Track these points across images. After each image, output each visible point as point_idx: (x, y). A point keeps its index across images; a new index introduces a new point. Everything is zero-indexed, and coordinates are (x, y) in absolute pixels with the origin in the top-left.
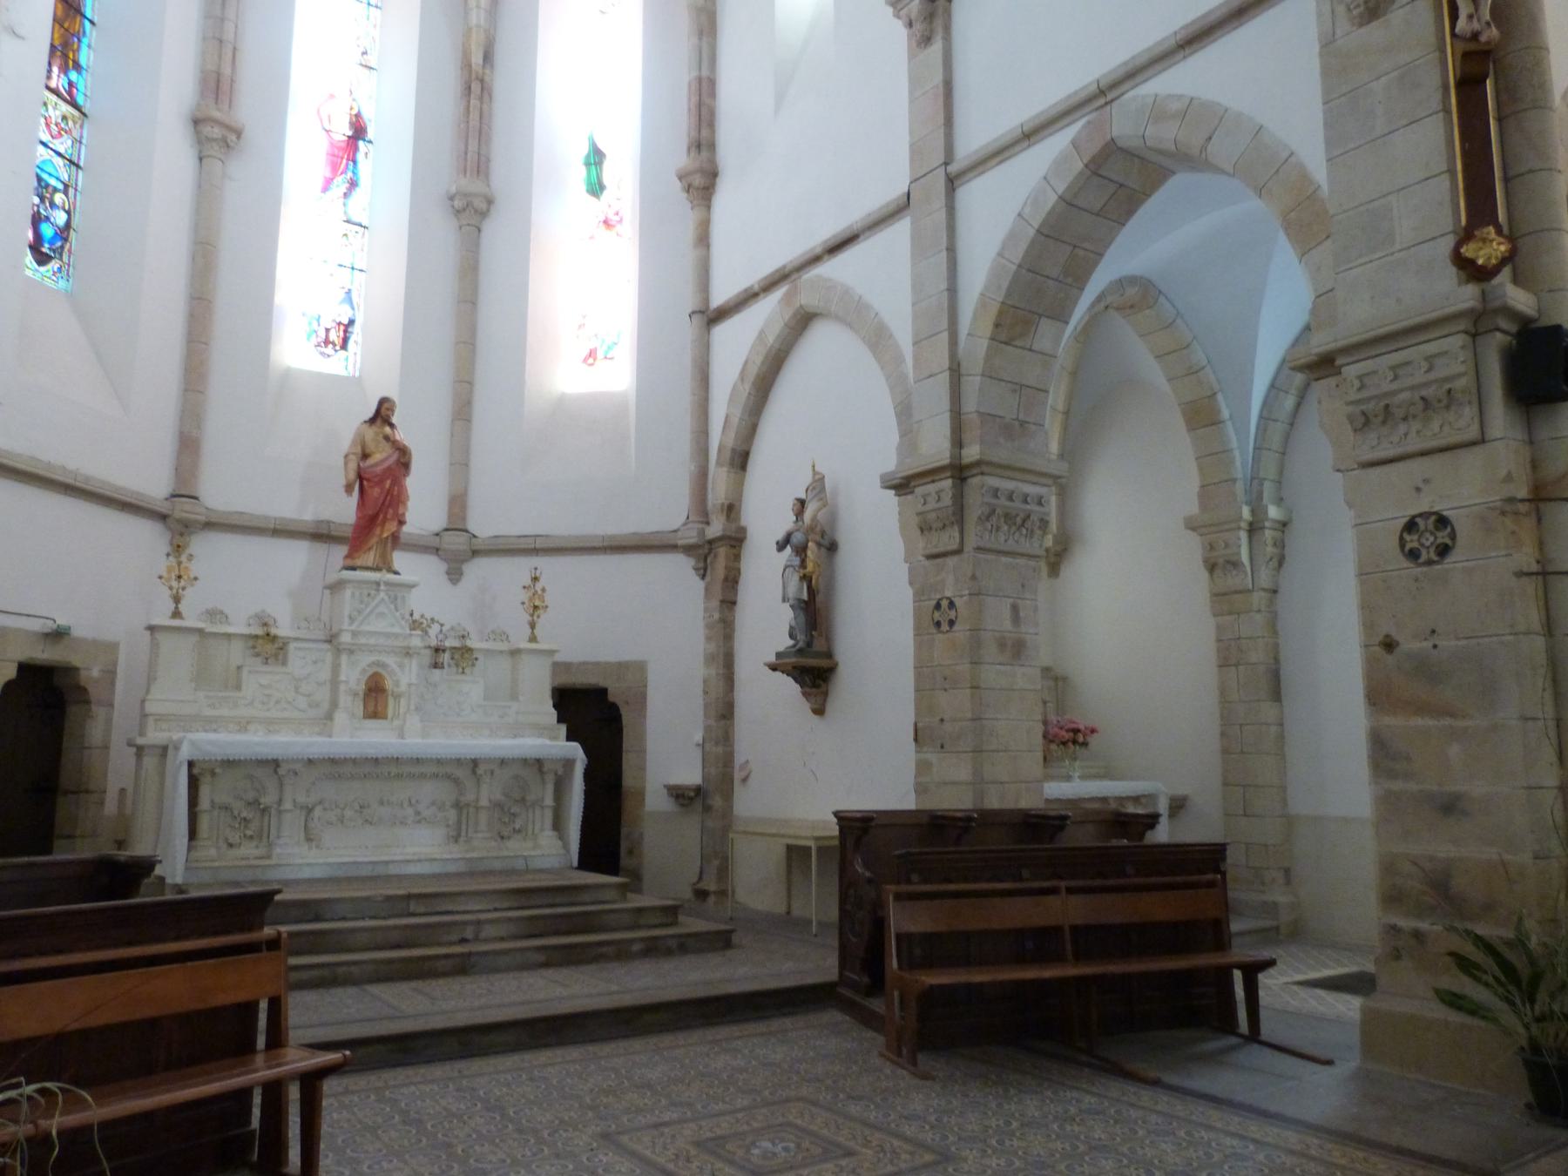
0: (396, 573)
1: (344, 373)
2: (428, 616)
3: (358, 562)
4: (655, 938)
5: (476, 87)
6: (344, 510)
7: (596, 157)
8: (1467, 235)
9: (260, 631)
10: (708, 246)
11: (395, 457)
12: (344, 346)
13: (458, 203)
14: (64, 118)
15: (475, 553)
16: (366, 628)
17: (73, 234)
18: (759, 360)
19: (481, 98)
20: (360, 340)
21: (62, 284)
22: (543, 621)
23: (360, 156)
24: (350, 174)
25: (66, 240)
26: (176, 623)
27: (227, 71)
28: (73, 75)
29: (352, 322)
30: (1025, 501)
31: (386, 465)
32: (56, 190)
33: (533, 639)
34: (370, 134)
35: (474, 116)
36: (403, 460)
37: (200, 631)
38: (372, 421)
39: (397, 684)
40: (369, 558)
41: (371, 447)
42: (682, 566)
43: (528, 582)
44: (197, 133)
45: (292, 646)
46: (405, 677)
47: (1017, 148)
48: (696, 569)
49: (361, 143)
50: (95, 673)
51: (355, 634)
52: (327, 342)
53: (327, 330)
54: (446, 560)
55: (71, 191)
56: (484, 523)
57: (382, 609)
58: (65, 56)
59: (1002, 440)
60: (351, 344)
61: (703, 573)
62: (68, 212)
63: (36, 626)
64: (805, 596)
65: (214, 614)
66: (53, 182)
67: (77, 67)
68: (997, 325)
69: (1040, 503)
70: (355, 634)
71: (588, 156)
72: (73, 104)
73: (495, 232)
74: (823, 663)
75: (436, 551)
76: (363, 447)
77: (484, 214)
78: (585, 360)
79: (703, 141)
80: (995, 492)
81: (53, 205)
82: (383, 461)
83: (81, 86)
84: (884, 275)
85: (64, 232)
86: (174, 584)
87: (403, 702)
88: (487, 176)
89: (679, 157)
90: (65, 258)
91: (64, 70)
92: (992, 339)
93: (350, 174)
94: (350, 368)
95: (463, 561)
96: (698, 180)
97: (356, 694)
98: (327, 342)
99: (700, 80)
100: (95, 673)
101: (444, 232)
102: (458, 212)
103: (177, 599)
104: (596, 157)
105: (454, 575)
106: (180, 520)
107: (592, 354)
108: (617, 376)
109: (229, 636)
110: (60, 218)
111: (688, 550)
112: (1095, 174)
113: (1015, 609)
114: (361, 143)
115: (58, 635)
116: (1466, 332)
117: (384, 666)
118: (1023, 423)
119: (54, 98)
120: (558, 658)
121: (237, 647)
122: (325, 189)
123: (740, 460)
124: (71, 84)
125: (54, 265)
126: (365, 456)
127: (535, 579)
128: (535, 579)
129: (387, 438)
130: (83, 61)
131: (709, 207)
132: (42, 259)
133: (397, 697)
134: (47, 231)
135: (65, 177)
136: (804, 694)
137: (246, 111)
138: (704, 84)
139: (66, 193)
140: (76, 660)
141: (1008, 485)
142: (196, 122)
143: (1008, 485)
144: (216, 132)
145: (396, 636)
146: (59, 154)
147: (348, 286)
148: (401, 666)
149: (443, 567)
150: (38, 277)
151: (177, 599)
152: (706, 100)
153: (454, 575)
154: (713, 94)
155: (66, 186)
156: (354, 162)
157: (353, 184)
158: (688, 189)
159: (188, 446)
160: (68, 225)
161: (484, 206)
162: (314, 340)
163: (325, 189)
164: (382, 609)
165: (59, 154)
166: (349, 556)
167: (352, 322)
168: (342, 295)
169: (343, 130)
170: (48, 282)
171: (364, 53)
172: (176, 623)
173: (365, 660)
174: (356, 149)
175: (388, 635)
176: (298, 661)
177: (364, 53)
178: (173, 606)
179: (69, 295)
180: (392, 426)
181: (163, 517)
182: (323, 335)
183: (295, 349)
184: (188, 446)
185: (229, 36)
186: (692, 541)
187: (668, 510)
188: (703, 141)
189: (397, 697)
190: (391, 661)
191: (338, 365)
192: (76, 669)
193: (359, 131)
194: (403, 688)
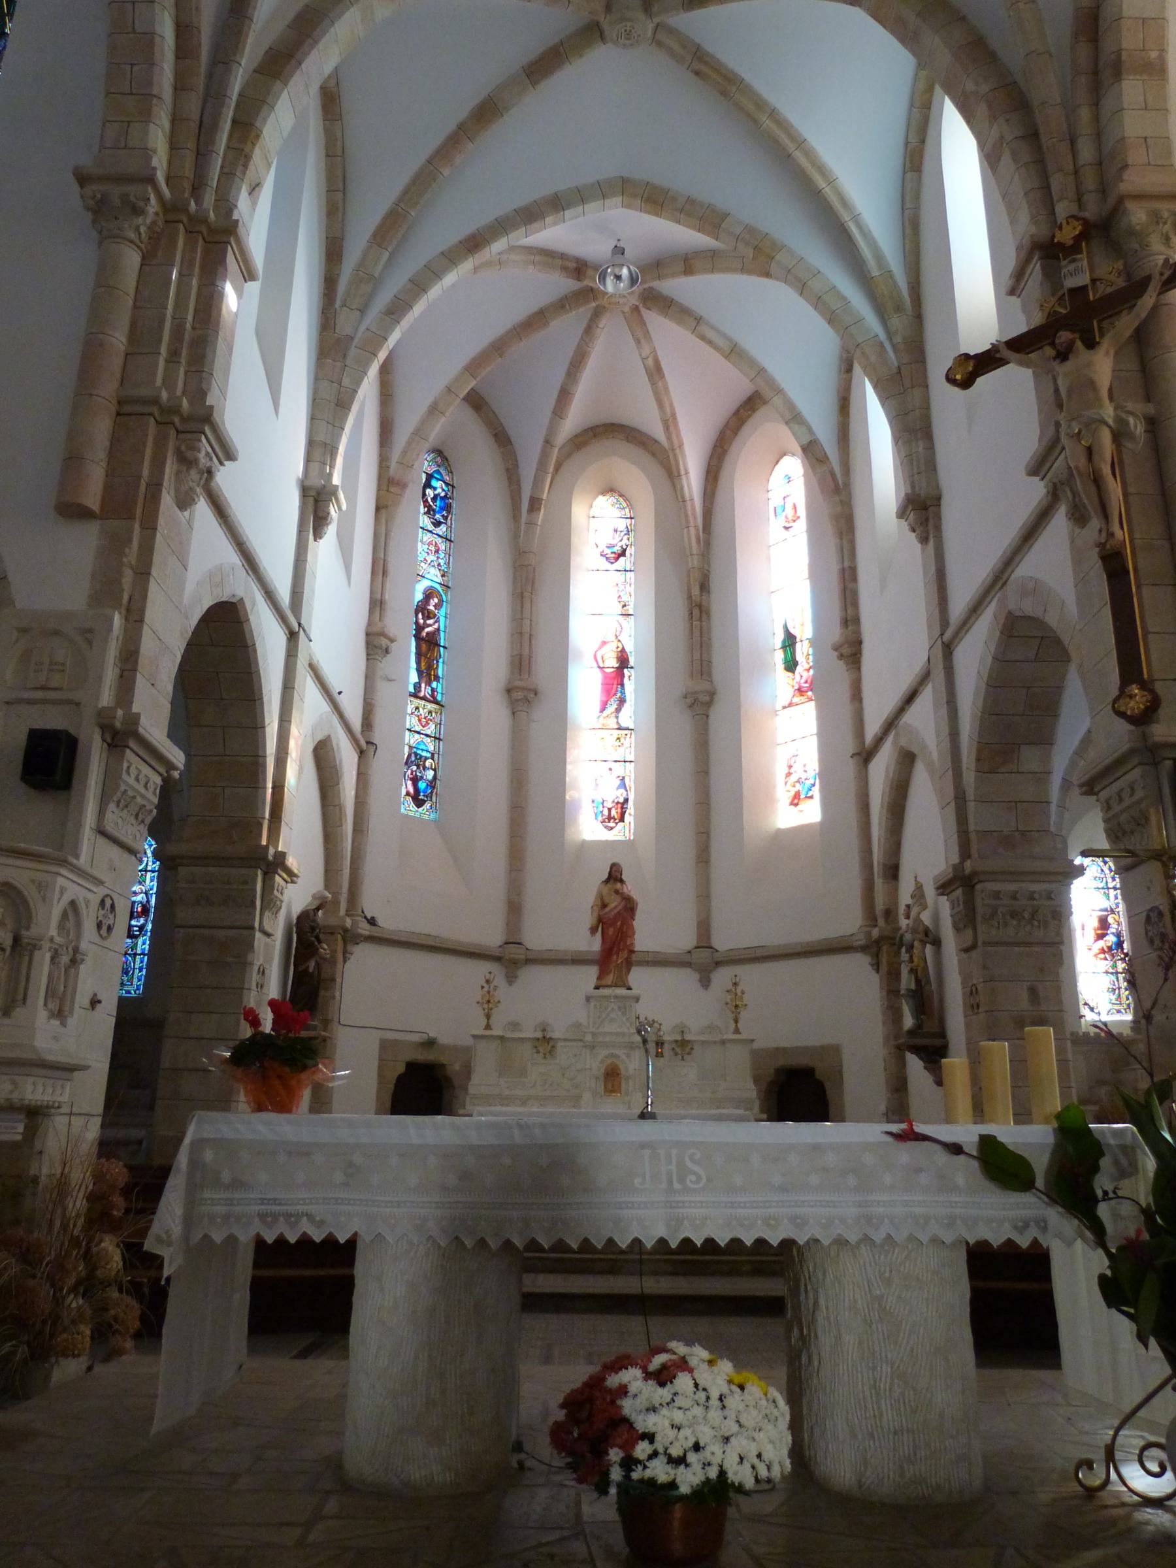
0: (629, 988)
1: (623, 838)
2: (650, 1018)
3: (603, 982)
4: (762, 1262)
5: (696, 612)
6: (595, 944)
7: (790, 641)
8: (1122, 692)
9: (539, 1035)
10: (860, 700)
11: (623, 903)
12: (622, 819)
13: (689, 701)
14: (430, 712)
15: (718, 964)
16: (601, 1030)
17: (438, 782)
18: (887, 790)
19: (700, 619)
20: (632, 812)
21: (433, 816)
22: (744, 1015)
23: (626, 680)
24: (619, 695)
25: (433, 787)
26: (488, 1033)
27: (526, 651)
28: (434, 685)
29: (626, 800)
30: (1032, 899)
31: (616, 911)
32: (426, 758)
33: (737, 1031)
34: (632, 662)
35: (697, 632)
36: (629, 907)
37: (502, 1038)
38: (607, 881)
39: (627, 1069)
40: (610, 979)
41: (607, 900)
42: (860, 963)
43: (730, 987)
44: (510, 697)
45: (560, 1044)
46: (632, 1064)
47: (971, 621)
48: (872, 965)
49: (626, 671)
50: (457, 1067)
51: (594, 1035)
52: (610, 818)
53: (610, 810)
54: (696, 970)
55: (436, 756)
56: (723, 941)
57: (612, 1016)
58: (429, 675)
59: (1001, 850)
60: (627, 817)
61: (877, 966)
62: (435, 770)
63: (416, 1038)
64: (913, 986)
65: (515, 1026)
66: (424, 754)
67: (437, 678)
68: (978, 760)
69: (1050, 898)
70: (594, 1035)
71: (784, 641)
72: (436, 702)
73: (718, 714)
74: (937, 1042)
75: (688, 964)
76: (602, 899)
77: (709, 704)
78: (792, 804)
79: (851, 620)
80: (997, 895)
81: (425, 768)
82: (615, 907)
83: (439, 690)
84: (924, 719)
85: (432, 784)
86: (486, 1006)
87: (631, 1083)
88: (709, 674)
89: (836, 633)
90: (434, 799)
91: (429, 683)
92: (977, 771)
93: (619, 695)
94: (627, 834)
95: (711, 971)
96: (846, 650)
97: (597, 1078)
98: (610, 818)
99: (843, 570)
100: (457, 1067)
101: (684, 725)
102: (691, 706)
103: (488, 1017)
104: (790, 641)
105: (705, 982)
106: (512, 958)
107: (797, 795)
108: (811, 813)
109: (522, 1040)
110: (430, 774)
111: (864, 949)
112: (1010, 636)
113: (1033, 991)
114: (626, 671)
115: (430, 1043)
116: (1139, 764)
117: (617, 1056)
118: (1023, 833)
119: (423, 702)
120: (756, 1045)
121: (528, 1048)
122: (603, 710)
123: (893, 872)
124: (433, 690)
125: (427, 805)
126: (604, 906)
127: (735, 984)
128: (735, 984)
129: (617, 892)
130: (440, 673)
131: (859, 669)
132: (419, 803)
133: (628, 1078)
134: (422, 785)
135: (431, 748)
136: (925, 1068)
137: (542, 674)
138: (847, 573)
139: (432, 758)
140: (443, 1059)
141: (1013, 887)
142: (509, 691)
143: (1013, 887)
144: (519, 695)
145: (624, 1035)
146: (427, 735)
147: (622, 774)
148: (628, 1056)
149: (696, 976)
150: (417, 815)
151: (488, 1017)
152: (850, 585)
153: (705, 982)
154: (854, 579)
155: (433, 754)
156: (622, 685)
157: (622, 701)
158: (841, 657)
159: (514, 909)
160: (435, 778)
161: (707, 698)
162: (600, 818)
163: (603, 710)
164: (612, 1016)
165: (427, 735)
166: (599, 978)
167: (626, 800)
168: (618, 782)
169: (612, 662)
170: (426, 817)
171: (624, 606)
172: (488, 1033)
173: (603, 1053)
174: (623, 676)
175: (617, 1034)
176: (563, 1054)
177: (624, 606)
178: (491, 1022)
179: (435, 821)
180: (622, 881)
181: (498, 959)
182: (606, 812)
183: (588, 828)
184: (514, 909)
185: (526, 629)
186: (862, 942)
187: (847, 920)
188: (851, 620)
189: (628, 1078)
190: (621, 1053)
191: (619, 833)
192: (443, 1065)
193: (623, 660)
194: (631, 1071)
